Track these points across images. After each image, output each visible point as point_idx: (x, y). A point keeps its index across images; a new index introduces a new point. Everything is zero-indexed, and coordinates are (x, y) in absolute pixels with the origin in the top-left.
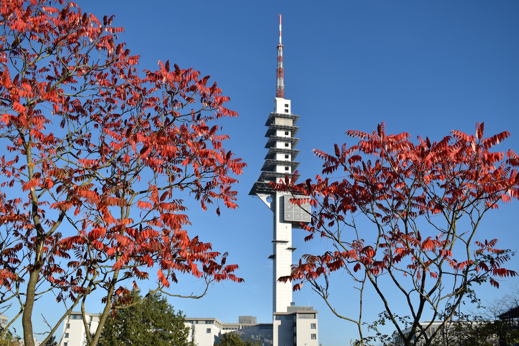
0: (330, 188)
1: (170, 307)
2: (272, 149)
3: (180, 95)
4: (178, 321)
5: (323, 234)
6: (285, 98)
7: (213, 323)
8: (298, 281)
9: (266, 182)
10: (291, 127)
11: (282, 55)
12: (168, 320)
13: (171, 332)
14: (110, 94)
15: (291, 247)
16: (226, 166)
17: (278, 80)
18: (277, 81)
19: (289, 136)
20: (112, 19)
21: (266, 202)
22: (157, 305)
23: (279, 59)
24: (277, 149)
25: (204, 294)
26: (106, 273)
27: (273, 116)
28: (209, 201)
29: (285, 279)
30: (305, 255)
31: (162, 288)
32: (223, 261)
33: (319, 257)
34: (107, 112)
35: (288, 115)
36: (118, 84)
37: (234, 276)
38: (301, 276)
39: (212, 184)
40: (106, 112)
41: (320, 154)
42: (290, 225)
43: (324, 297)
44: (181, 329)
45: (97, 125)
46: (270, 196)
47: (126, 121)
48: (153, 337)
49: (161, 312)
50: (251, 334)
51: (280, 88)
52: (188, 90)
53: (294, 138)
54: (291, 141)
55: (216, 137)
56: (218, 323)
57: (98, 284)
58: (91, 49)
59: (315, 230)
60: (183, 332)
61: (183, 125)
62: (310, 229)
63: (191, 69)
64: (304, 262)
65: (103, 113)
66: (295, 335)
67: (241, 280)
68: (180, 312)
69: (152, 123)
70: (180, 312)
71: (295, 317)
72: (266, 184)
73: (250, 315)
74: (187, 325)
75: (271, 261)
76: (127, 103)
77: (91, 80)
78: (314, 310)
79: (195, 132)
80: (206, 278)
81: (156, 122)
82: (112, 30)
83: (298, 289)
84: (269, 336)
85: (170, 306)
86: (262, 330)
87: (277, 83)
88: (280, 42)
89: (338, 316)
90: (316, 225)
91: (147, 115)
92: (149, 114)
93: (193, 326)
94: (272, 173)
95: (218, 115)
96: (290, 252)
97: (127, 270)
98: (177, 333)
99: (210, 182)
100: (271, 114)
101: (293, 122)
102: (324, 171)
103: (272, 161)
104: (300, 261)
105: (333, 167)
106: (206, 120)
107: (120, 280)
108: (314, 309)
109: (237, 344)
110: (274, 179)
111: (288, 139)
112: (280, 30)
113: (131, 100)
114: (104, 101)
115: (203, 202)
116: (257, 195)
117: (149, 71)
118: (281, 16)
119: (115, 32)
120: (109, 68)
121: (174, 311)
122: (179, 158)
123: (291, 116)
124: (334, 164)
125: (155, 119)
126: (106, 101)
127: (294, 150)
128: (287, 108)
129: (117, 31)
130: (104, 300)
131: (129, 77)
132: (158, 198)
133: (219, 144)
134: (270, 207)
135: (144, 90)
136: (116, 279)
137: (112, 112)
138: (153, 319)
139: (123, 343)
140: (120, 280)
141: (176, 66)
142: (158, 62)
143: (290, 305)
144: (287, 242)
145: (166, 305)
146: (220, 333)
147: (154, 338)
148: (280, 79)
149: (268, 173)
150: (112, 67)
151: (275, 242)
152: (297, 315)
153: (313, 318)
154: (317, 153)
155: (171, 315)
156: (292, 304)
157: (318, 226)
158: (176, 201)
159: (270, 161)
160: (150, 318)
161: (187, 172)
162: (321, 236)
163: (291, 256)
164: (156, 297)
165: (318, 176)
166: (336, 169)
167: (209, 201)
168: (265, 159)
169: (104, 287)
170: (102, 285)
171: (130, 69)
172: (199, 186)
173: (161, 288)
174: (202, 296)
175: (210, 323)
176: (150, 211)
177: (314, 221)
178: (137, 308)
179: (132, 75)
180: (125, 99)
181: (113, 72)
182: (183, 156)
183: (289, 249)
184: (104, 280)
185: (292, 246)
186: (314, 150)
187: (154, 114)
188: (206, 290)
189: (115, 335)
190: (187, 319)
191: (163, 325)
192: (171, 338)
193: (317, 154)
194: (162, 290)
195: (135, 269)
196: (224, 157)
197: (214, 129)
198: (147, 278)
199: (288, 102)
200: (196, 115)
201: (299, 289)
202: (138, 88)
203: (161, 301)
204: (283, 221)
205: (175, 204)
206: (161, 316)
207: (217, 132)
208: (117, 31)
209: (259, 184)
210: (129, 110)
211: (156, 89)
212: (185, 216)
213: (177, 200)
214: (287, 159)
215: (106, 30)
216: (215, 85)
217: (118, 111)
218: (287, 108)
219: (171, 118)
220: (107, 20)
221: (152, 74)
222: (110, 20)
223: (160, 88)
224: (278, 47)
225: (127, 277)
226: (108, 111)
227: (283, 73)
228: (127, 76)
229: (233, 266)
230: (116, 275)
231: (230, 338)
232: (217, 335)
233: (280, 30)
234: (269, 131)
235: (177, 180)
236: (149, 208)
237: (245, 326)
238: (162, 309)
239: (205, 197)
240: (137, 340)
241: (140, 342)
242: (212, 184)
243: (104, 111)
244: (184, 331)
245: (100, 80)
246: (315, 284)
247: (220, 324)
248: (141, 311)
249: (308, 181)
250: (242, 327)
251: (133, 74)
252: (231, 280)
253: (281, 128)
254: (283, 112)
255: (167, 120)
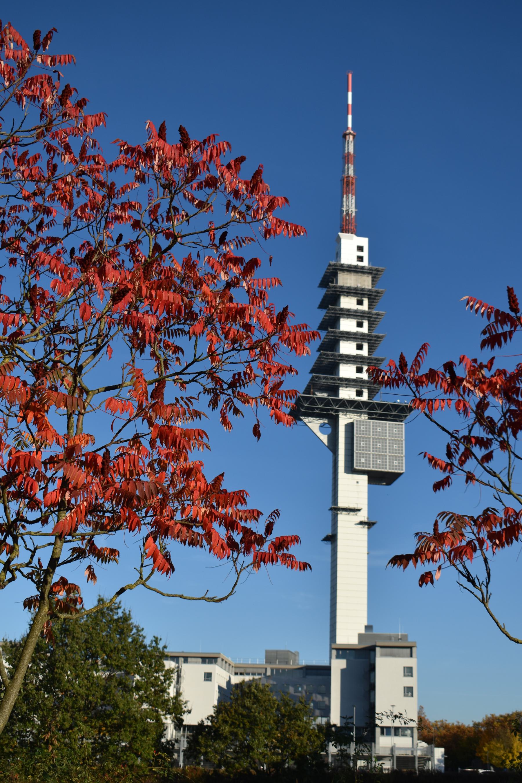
0: (494, 380)
1: (138, 630)
2: (332, 332)
3: (185, 195)
4: (151, 656)
5: (470, 477)
6: (358, 235)
7: (216, 662)
8: (429, 567)
9: (319, 395)
10: (369, 290)
11: (351, 150)
12: (133, 655)
13: (137, 677)
14: (44, 193)
15: (366, 520)
16: (274, 340)
17: (345, 199)
18: (342, 202)
19: (365, 307)
20: (51, 37)
21: (319, 434)
22: (113, 626)
23: (346, 158)
24: (342, 333)
25: (230, 594)
26: (36, 549)
27: (334, 269)
28: (236, 411)
29: (405, 561)
30: (443, 513)
31: (146, 580)
32: (269, 529)
33: (472, 518)
34: (35, 233)
35: (363, 268)
36: (59, 173)
37: (293, 557)
38: (436, 556)
39: (243, 378)
40: (32, 233)
41: (478, 305)
42: (365, 478)
43: (483, 601)
44: (157, 672)
45: (15, 259)
46: (326, 421)
47: (72, 251)
48: (105, 686)
49: (120, 639)
50: (288, 685)
51: (348, 214)
52: (200, 186)
53: (374, 312)
54: (369, 317)
55: (256, 282)
56: (226, 662)
57: (20, 571)
58: (6, 103)
59: (455, 469)
60: (162, 678)
61: (189, 258)
62: (444, 465)
63: (214, 136)
64: (442, 528)
65: (26, 235)
66: (372, 687)
67: (305, 566)
68: (156, 640)
69: (125, 255)
70: (156, 640)
71: (372, 653)
72: (319, 399)
73: (287, 649)
74: (169, 664)
75: (328, 546)
76: (76, 214)
77: (5, 168)
78: (411, 640)
79: (213, 272)
80: (234, 562)
81: (133, 253)
82: (49, 59)
83: (429, 583)
84: (323, 688)
85: (137, 627)
86: (310, 678)
87: (342, 206)
88: (350, 125)
89: (511, 639)
90: (458, 457)
91: (115, 238)
92: (120, 237)
93: (178, 667)
94: (332, 379)
95: (267, 232)
96: (364, 530)
97: (77, 544)
98: (149, 679)
99: (239, 374)
100: (330, 265)
101: (373, 281)
102: (484, 344)
103: (332, 355)
104: (436, 524)
105: (504, 335)
106: (239, 243)
107: (63, 563)
108: (410, 639)
109: (265, 702)
110: (334, 390)
111: (363, 312)
112: (350, 102)
113: (83, 209)
114: (31, 210)
115: (225, 414)
116: (301, 420)
117: (126, 143)
118: (350, 76)
119: (57, 64)
120: (42, 140)
121: (144, 637)
122: (179, 324)
123: (370, 269)
124: (507, 328)
125: (132, 247)
126: (34, 211)
127: (374, 334)
128: (360, 254)
129: (60, 61)
130: (28, 603)
131: (82, 159)
132: (146, 392)
133: (262, 295)
134: (327, 444)
135: (112, 187)
136: (58, 559)
137: (46, 233)
138: (105, 652)
139: (46, 696)
140: (63, 563)
141: (182, 131)
142: (146, 123)
143: (363, 631)
144: (359, 510)
145: (129, 625)
146: (229, 683)
147: (106, 689)
148: (348, 198)
149: (324, 379)
150: (48, 138)
151: (335, 510)
152: (378, 650)
153: (407, 657)
154: (471, 303)
155: (138, 644)
156: (368, 628)
157: (460, 459)
158: (180, 400)
159: (328, 355)
160: (99, 649)
161: (197, 350)
162: (467, 482)
163: (365, 538)
164: (112, 610)
165: (464, 357)
166: (511, 338)
167: (236, 411)
168: (319, 350)
169: (29, 576)
170: (25, 574)
171: (85, 141)
172: (218, 381)
173: (144, 579)
174: (226, 598)
175: (210, 662)
176: (130, 420)
177: (452, 450)
178: (76, 631)
179: (88, 155)
180: (71, 206)
181: (50, 149)
182: (186, 320)
183: (361, 523)
184: (30, 562)
185: (368, 518)
186: (466, 298)
187: (130, 235)
188: (235, 585)
189: (31, 682)
190: (170, 654)
191: (122, 663)
192: (138, 688)
193: (472, 307)
194: (147, 583)
195: (91, 543)
196: (272, 322)
197: (254, 263)
198: (115, 560)
199: (364, 242)
200: (218, 234)
201: (432, 582)
202: (99, 182)
203: (119, 618)
204: (351, 469)
205: (178, 406)
206: (120, 646)
207: (257, 273)
208: (60, 61)
209: (306, 399)
210: (79, 228)
211: (137, 185)
212: (201, 433)
213: (182, 398)
214: (359, 352)
215: (39, 60)
216: (258, 173)
217: (58, 231)
218: (360, 254)
219: (164, 243)
220: (42, 39)
221: (130, 150)
222: (46, 39)
223: (144, 182)
224: (345, 136)
225: (77, 558)
226: (38, 231)
227: (354, 187)
228: (78, 159)
229: (290, 539)
230: (58, 551)
231: (250, 690)
232: (224, 686)
233: (350, 102)
234: (326, 297)
235: (175, 367)
236: (128, 413)
237: (278, 670)
238: (121, 633)
239: (229, 402)
240: (74, 691)
241: (79, 695)
242: (243, 378)
243: (29, 230)
244: (164, 676)
245: (22, 168)
246: (464, 573)
247: (230, 665)
248: (84, 636)
249: (449, 366)
250: (272, 670)
251: (90, 152)
252: (284, 567)
253: (350, 292)
254: (354, 262)
255: (157, 247)
